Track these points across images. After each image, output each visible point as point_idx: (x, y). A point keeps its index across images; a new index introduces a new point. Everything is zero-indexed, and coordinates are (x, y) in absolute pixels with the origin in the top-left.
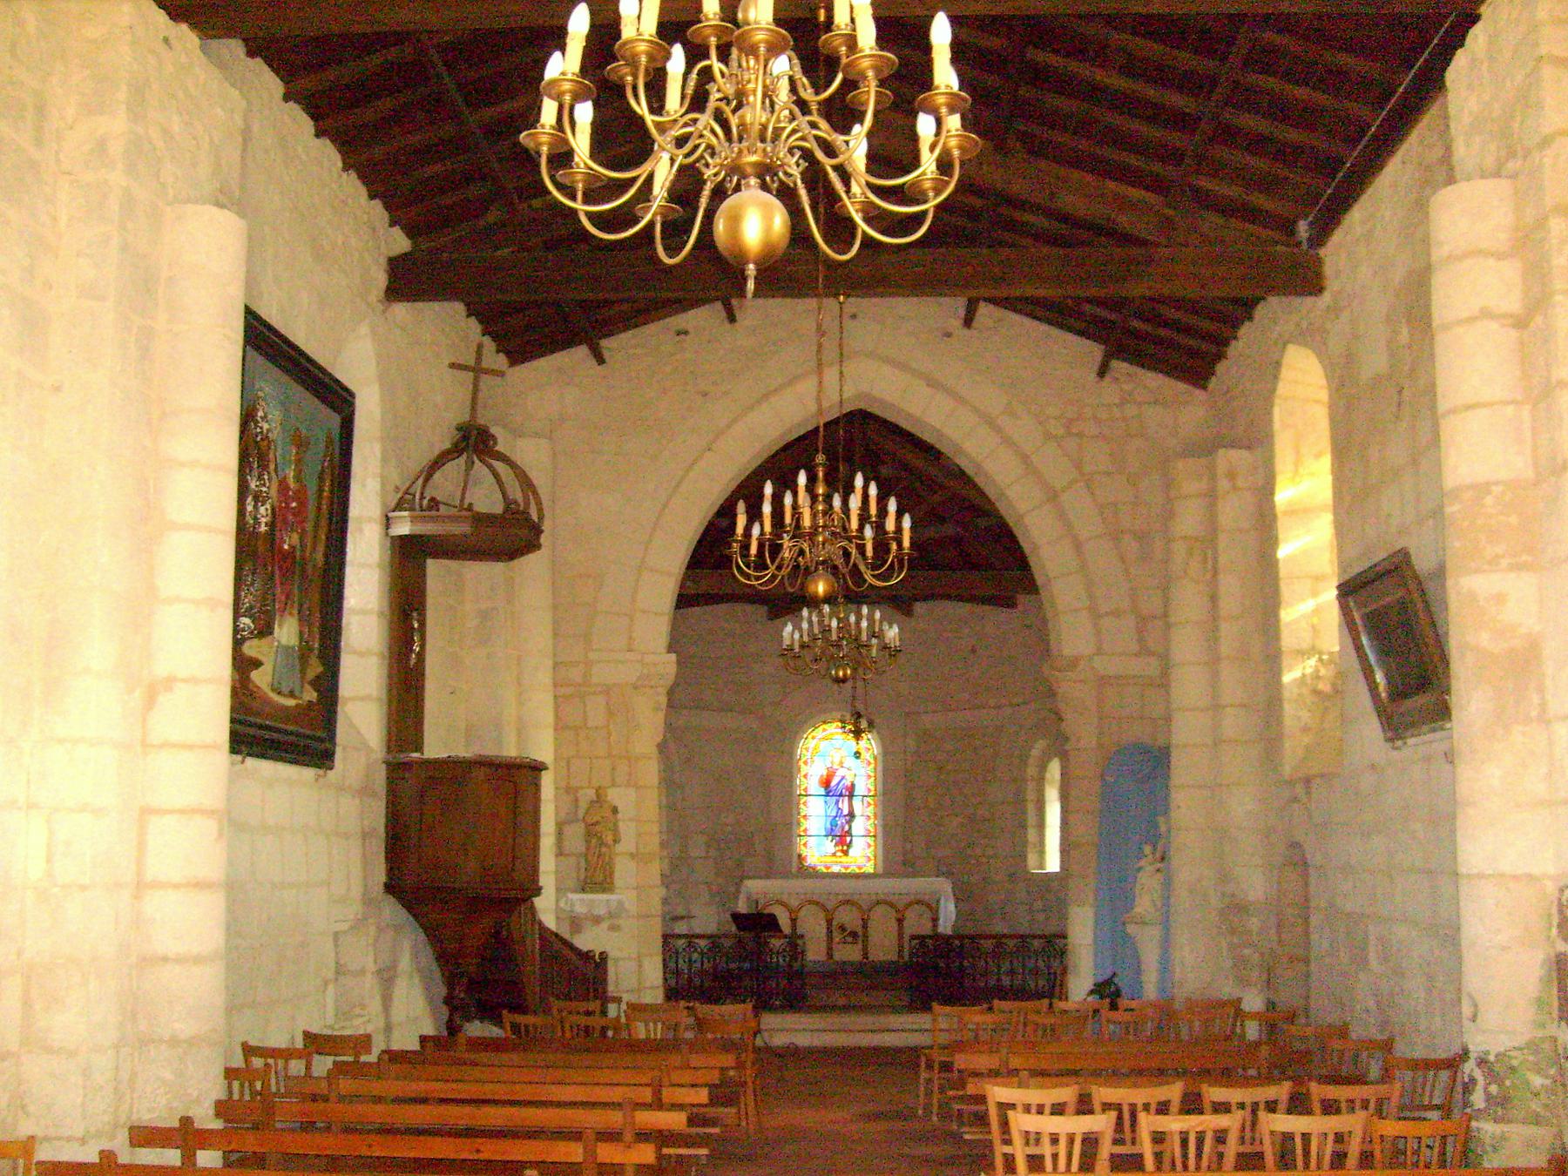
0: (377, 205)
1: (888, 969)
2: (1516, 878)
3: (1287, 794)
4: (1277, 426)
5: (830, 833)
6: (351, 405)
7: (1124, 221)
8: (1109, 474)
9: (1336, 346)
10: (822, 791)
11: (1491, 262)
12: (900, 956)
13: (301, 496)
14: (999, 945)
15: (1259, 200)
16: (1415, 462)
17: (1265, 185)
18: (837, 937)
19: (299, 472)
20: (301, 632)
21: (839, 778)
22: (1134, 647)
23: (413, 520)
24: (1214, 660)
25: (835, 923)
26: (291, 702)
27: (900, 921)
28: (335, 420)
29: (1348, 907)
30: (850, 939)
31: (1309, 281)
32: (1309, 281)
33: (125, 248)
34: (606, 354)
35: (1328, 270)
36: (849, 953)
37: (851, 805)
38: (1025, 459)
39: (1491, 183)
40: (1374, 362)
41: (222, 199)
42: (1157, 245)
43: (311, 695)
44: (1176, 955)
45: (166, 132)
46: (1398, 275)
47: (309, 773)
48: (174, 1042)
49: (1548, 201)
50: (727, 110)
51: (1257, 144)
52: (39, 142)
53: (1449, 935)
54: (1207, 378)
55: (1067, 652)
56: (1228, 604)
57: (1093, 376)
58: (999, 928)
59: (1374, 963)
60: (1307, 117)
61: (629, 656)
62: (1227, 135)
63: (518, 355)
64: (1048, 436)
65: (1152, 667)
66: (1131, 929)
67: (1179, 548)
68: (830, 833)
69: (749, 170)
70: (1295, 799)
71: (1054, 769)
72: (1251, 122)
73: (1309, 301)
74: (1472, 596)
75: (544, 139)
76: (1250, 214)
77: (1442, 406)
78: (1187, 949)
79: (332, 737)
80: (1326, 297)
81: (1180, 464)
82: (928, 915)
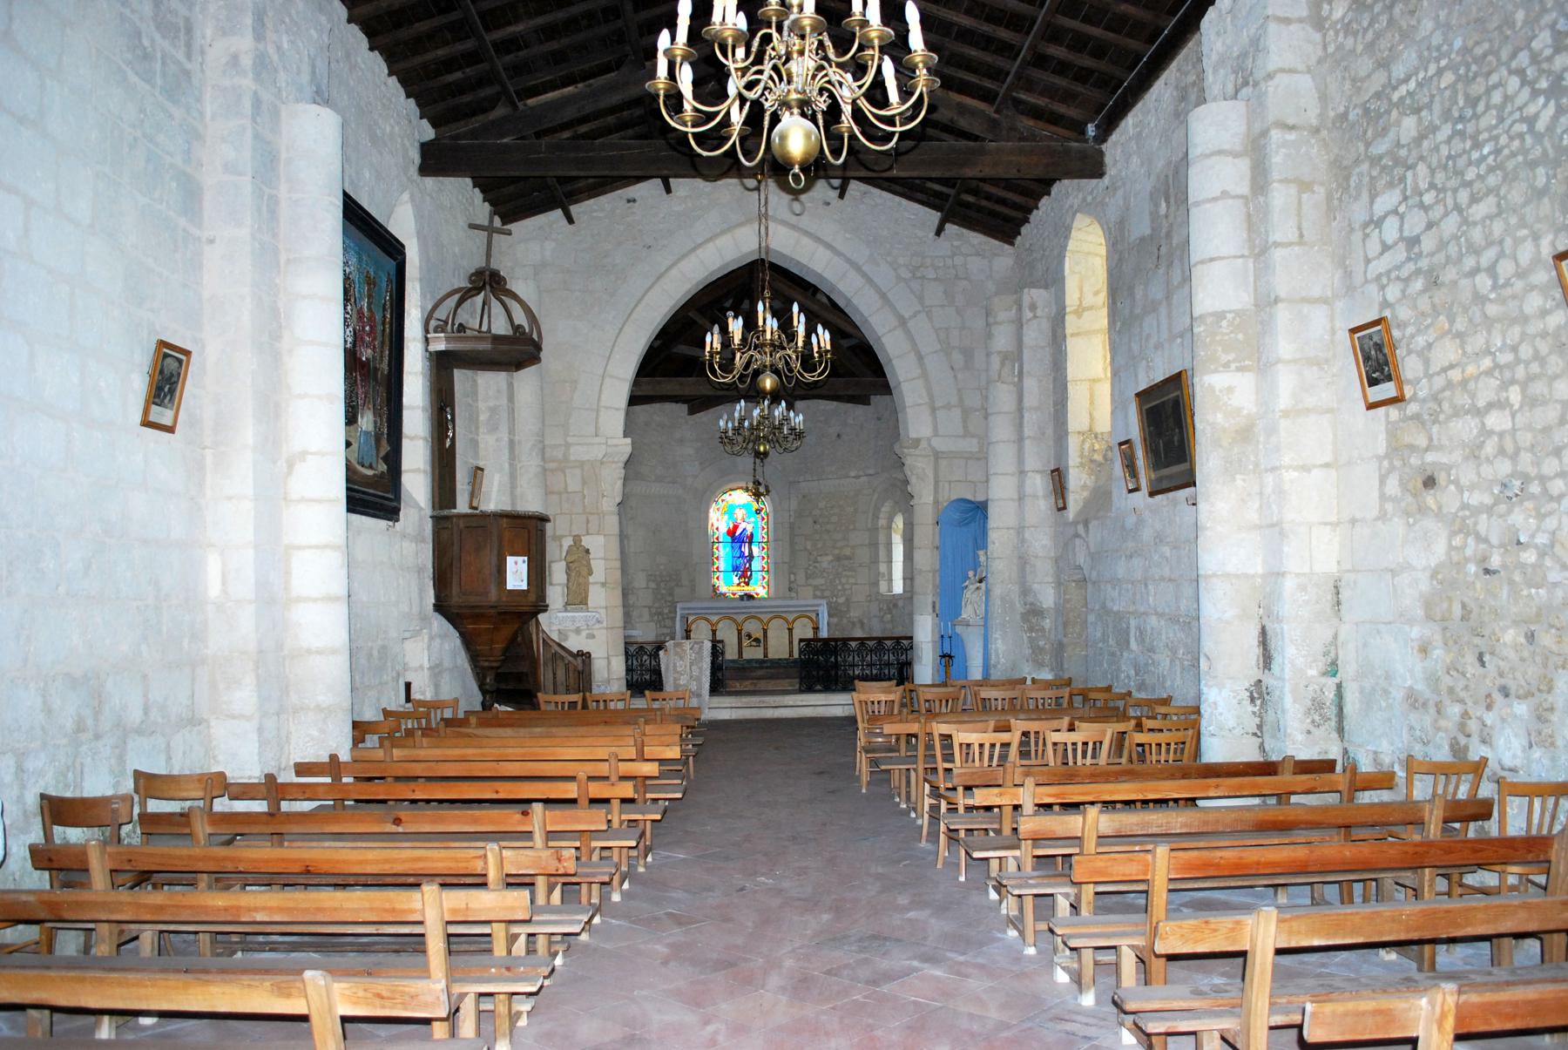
0: (412, 101)
1: (777, 663)
2: (1237, 576)
3: (1071, 531)
4: (1067, 272)
5: (735, 569)
6: (403, 254)
7: (963, 123)
8: (942, 306)
9: (1113, 213)
10: (729, 539)
11: (1230, 159)
13: (371, 319)
14: (862, 644)
15: (1061, 109)
16: (1168, 297)
17: (1068, 97)
18: (745, 643)
19: (369, 304)
20: (375, 422)
22: (961, 431)
23: (448, 339)
24: (1020, 440)
26: (370, 473)
27: (790, 630)
28: (391, 265)
29: (1115, 609)
31: (1093, 167)
32: (1093, 167)
33: (256, 136)
35: (1108, 160)
36: (757, 654)
37: (750, 549)
38: (883, 296)
39: (1231, 103)
40: (1140, 227)
41: (318, 99)
42: (984, 139)
43: (383, 467)
44: (992, 647)
45: (279, 48)
46: (1160, 164)
47: (383, 524)
48: (319, 709)
49: (1271, 116)
50: (779, 64)
51: (1062, 68)
52: (189, 57)
53: (1191, 622)
54: (1015, 237)
55: (913, 435)
56: (1029, 401)
57: (932, 234)
58: (859, 634)
59: (1133, 645)
60: (1099, 51)
61: (597, 440)
62: (1040, 61)
63: (508, 218)
64: (899, 278)
65: (971, 445)
66: (959, 629)
67: (996, 361)
68: (735, 569)
69: (793, 103)
70: (1077, 535)
71: (899, 522)
72: (1057, 52)
73: (1094, 182)
74: (1211, 388)
75: (661, 86)
76: (1054, 119)
77: (1194, 258)
78: (1000, 641)
79: (398, 498)
80: (1106, 180)
81: (996, 300)
82: (811, 625)
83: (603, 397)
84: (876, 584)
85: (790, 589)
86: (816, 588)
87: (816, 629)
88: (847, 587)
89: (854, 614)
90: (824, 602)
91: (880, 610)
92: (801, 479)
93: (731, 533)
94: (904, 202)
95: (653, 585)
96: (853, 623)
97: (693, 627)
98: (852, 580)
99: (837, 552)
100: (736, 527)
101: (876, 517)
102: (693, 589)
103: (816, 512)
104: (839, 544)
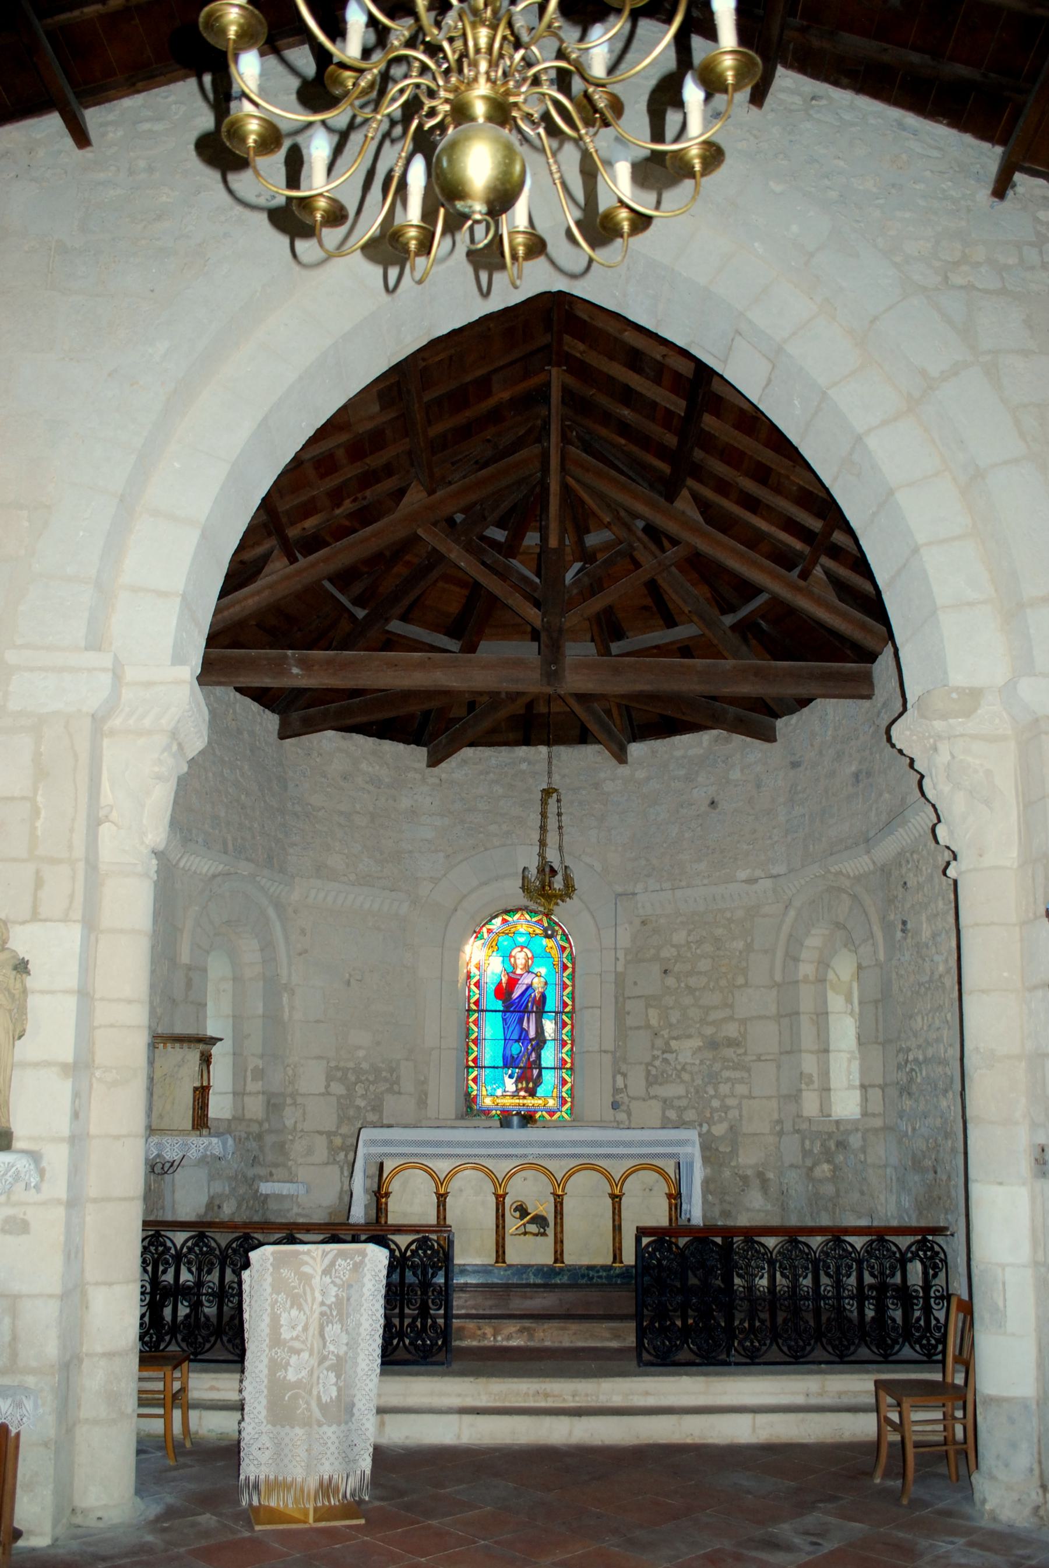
5: (509, 1062)
10: (499, 1005)
12: (617, 1255)
18: (513, 1224)
21: (524, 987)
25: (508, 1201)
27: (616, 1199)
30: (533, 1228)
34: (93, 134)
55: (957, 678)
57: (984, 194)
61: (91, 659)
68: (509, 1062)
83: (549, 1066)
84: (795, 1097)
85: (615, 1106)
86: (667, 1103)
87: (675, 1198)
88: (731, 1102)
89: (748, 1158)
90: (693, 1135)
91: (806, 1153)
92: (639, 888)
93: (503, 992)
94: (911, 119)
95: (338, 1089)
96: (745, 1179)
97: (395, 1186)
98: (741, 1089)
99: (709, 1031)
100: (513, 982)
101: (793, 958)
102: (422, 1102)
103: (667, 953)
104: (715, 1015)
